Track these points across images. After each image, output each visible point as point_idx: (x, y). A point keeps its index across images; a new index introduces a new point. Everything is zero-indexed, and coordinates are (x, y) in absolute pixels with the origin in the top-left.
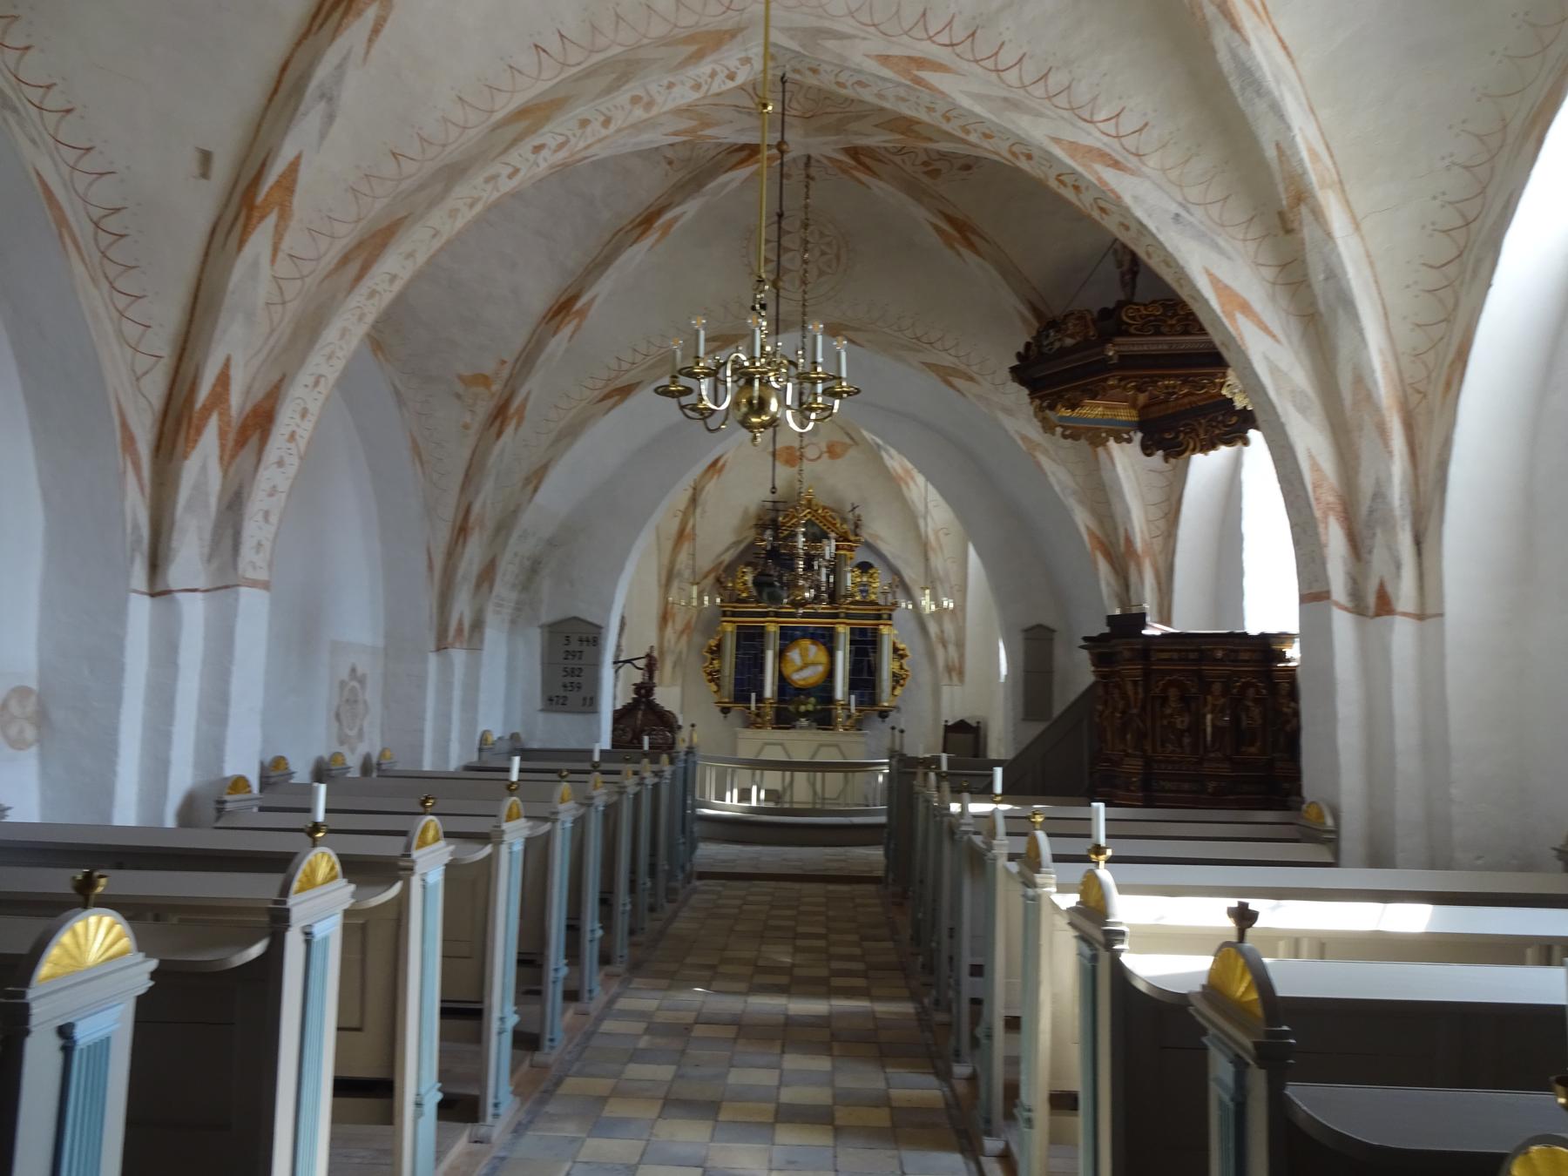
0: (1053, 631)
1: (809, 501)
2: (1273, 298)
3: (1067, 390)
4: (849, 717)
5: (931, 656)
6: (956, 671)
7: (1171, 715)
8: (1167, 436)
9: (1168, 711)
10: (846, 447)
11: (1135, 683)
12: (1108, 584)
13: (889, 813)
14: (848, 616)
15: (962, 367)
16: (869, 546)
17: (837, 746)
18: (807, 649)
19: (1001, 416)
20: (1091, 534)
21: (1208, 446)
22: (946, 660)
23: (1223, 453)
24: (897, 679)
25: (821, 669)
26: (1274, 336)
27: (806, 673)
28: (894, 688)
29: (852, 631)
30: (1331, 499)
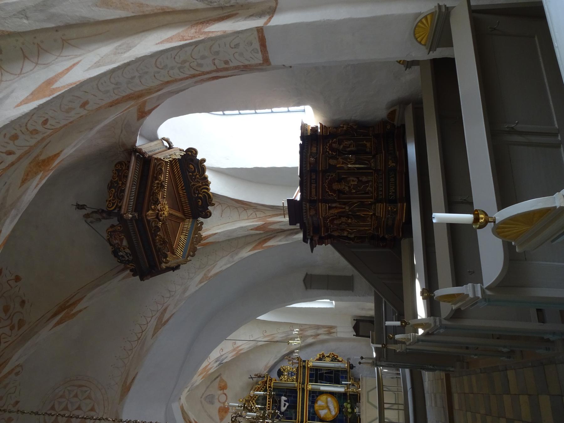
0: (307, 274)
1: (246, 401)
2: (47, 65)
3: (155, 246)
4: (353, 385)
5: (323, 342)
6: (330, 329)
7: (349, 187)
8: (200, 203)
9: (347, 188)
10: (222, 380)
11: (330, 208)
12: (280, 241)
13: (404, 367)
14: (303, 383)
15: (158, 314)
16: (270, 370)
17: (368, 392)
18: (320, 406)
19: (188, 294)
20: (254, 248)
21: (207, 183)
22: (325, 334)
23: (207, 173)
24: (334, 359)
25: (329, 399)
26: (74, 65)
27: (332, 407)
28: (339, 361)
29: (311, 381)
30: (193, 31)
